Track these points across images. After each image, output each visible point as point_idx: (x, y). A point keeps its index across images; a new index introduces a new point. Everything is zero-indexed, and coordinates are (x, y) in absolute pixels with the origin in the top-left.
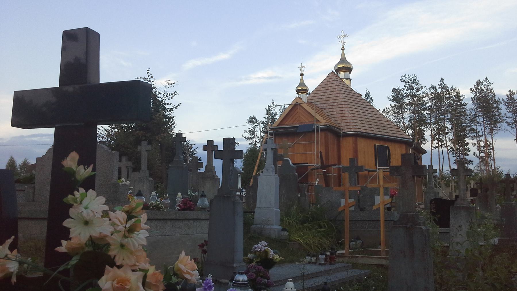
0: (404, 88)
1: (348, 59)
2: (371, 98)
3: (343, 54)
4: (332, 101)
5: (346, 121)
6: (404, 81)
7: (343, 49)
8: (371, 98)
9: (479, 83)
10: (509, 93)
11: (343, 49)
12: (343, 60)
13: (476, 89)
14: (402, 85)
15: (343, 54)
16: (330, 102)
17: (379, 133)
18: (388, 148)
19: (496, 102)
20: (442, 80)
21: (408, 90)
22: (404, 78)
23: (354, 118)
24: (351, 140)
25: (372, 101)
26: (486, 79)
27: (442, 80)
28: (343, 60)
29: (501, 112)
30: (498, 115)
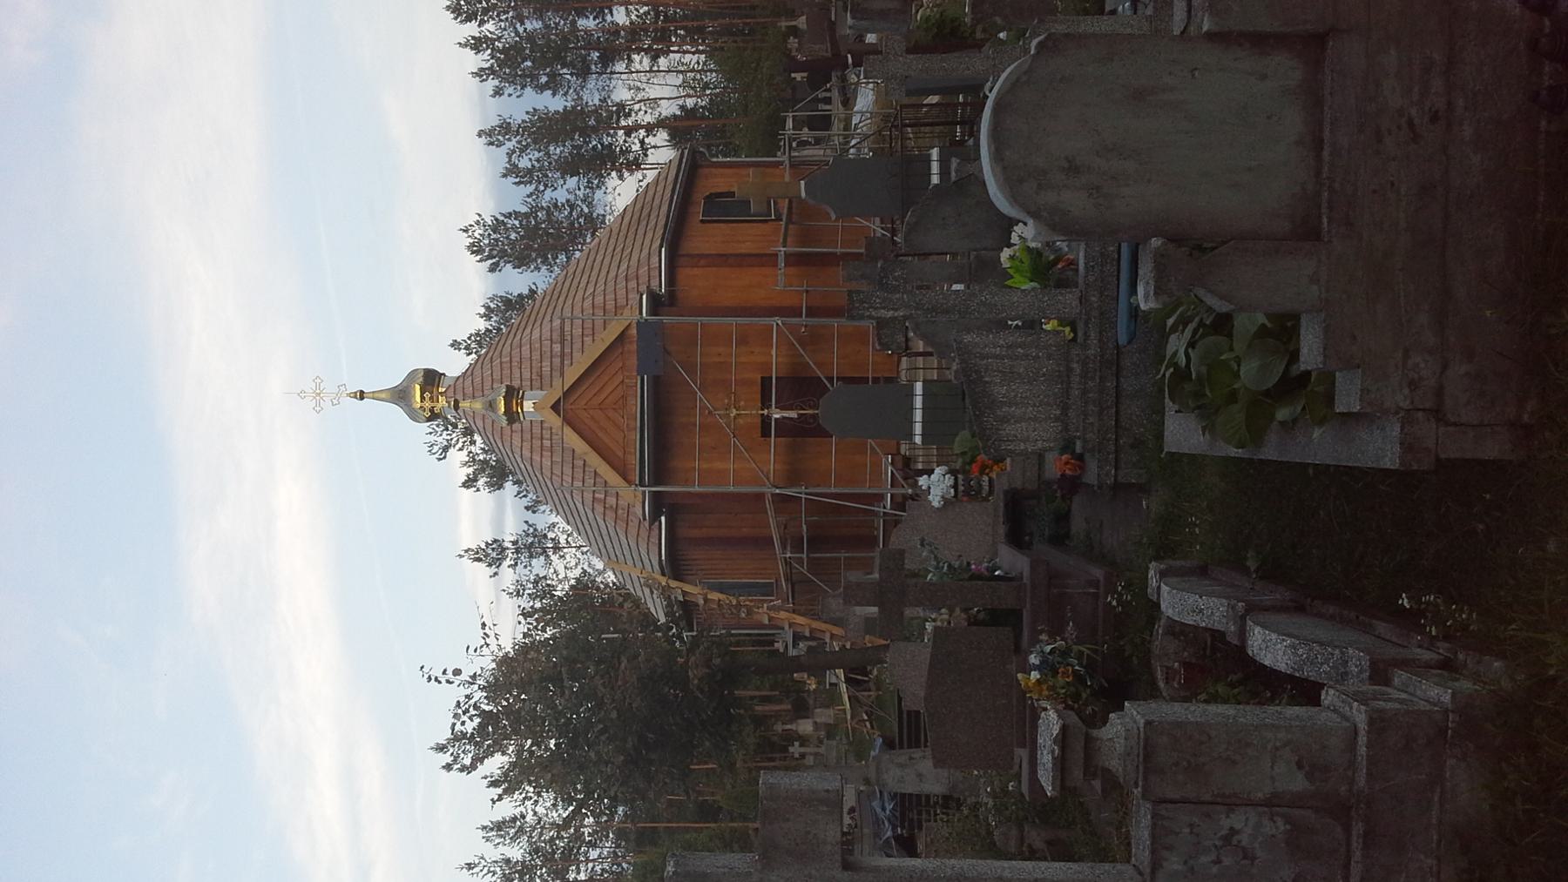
0: (465, 452)
1: (396, 380)
2: (487, 544)
3: (375, 396)
4: (546, 363)
5: (621, 293)
6: (445, 449)
7: (362, 395)
8: (487, 544)
9: (475, 249)
10: (511, 179)
11: (362, 395)
12: (399, 396)
13: (490, 257)
14: (457, 456)
15: (375, 396)
16: (546, 369)
17: (665, 208)
18: (710, 199)
19: (534, 210)
20: (455, 345)
21: (473, 442)
22: (436, 448)
23: (612, 274)
24: (684, 273)
25: (495, 541)
26: (466, 231)
27: (455, 345)
28: (399, 396)
29: (562, 200)
30: (572, 207)
